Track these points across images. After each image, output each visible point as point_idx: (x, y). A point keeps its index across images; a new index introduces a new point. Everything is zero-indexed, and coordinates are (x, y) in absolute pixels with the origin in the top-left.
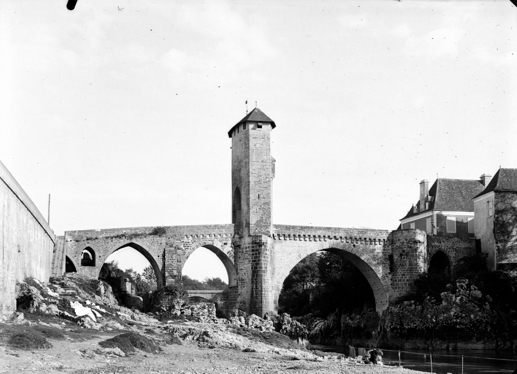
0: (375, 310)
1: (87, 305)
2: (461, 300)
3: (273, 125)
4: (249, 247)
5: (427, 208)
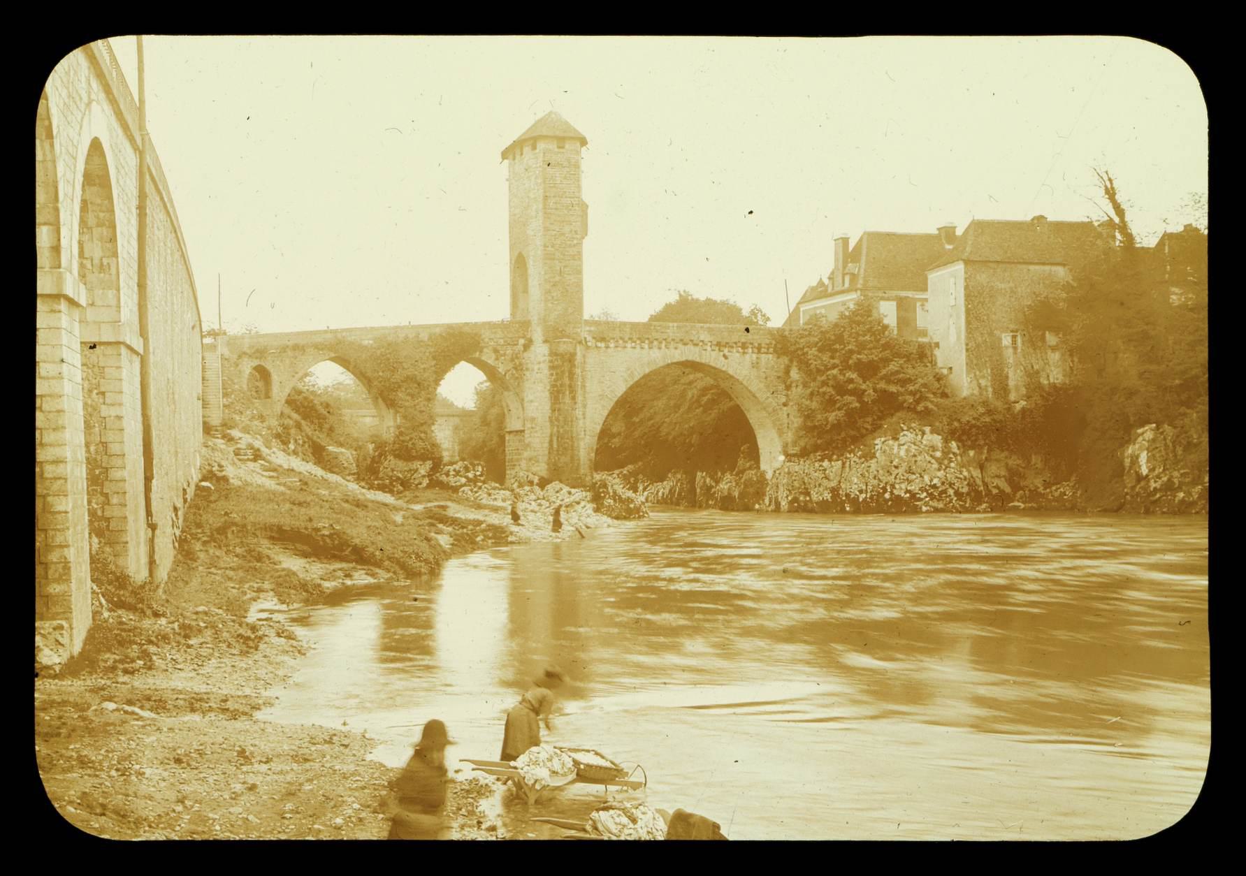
0: (758, 468)
1: (783, 512)
2: (907, 451)
3: (583, 142)
4: (544, 361)
5: (847, 285)
